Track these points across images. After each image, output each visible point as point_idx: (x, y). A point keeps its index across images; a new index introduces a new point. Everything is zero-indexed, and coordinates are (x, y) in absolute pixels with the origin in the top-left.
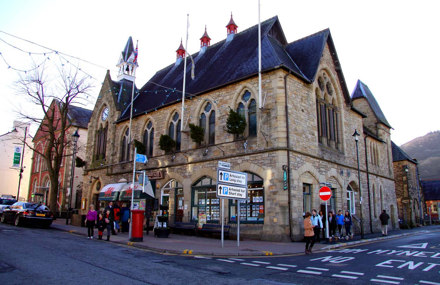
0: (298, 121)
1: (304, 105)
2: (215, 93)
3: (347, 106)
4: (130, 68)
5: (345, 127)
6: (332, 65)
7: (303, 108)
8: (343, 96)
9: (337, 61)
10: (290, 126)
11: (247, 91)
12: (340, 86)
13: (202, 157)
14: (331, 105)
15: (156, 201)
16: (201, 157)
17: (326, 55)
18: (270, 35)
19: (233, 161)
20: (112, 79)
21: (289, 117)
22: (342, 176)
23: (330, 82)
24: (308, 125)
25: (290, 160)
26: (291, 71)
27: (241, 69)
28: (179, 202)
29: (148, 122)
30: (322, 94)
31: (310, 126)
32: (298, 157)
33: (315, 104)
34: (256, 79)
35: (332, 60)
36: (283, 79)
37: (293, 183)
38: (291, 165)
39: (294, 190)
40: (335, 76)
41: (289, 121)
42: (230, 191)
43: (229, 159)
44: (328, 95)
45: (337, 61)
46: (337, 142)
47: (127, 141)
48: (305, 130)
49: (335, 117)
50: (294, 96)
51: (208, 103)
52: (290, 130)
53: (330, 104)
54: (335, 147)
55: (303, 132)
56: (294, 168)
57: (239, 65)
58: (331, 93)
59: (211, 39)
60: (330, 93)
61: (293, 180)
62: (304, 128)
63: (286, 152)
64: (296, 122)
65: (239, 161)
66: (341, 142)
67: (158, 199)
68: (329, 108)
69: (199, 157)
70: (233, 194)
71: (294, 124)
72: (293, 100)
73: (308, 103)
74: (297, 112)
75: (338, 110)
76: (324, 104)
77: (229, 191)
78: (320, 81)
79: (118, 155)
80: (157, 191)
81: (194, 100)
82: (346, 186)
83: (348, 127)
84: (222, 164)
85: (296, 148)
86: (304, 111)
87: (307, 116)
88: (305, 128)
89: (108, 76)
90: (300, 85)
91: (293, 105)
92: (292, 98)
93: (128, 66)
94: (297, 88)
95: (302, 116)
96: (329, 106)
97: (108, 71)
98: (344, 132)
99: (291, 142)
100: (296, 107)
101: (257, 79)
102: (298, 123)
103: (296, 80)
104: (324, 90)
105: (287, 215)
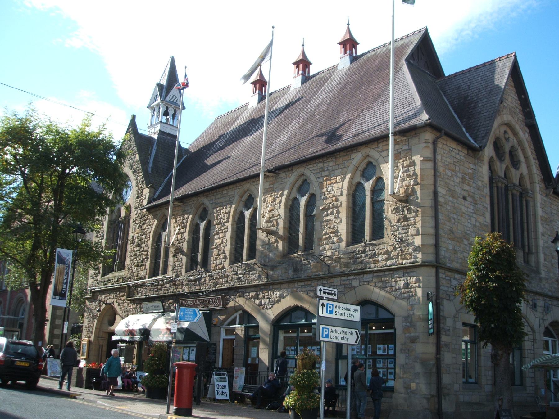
0: (455, 217)
1: (466, 187)
2: (315, 165)
3: (547, 188)
4: (171, 112)
5: (542, 224)
6: (521, 116)
7: (466, 194)
8: (540, 170)
9: (528, 110)
10: (441, 226)
11: (370, 163)
12: (534, 152)
13: (292, 273)
14: (516, 187)
15: (212, 347)
16: (291, 273)
17: (510, 99)
18: (414, 60)
19: (344, 283)
20: (140, 131)
21: (439, 211)
22: (535, 312)
23: (517, 146)
24: (474, 223)
25: (441, 284)
26: (445, 131)
27: (361, 124)
28: (252, 351)
29: (201, 210)
30: (500, 168)
31: (478, 224)
32: (454, 279)
33: (488, 186)
34: (385, 143)
35: (520, 107)
36: (430, 145)
37: (445, 323)
38: (441, 292)
39: (446, 335)
40: (524, 136)
41: (440, 216)
42: (336, 310)
43: (337, 281)
44: (513, 170)
45: (528, 110)
46: (527, 250)
47: (163, 241)
48: (468, 232)
49: (525, 208)
50: (449, 173)
51: (305, 181)
52: (441, 232)
53: (514, 185)
54: (522, 259)
55: (466, 236)
56: (448, 298)
57: (358, 116)
58: (517, 164)
59: (311, 64)
60: (515, 164)
61: (445, 318)
62: (465, 227)
63: (433, 270)
64: (452, 219)
65: (355, 283)
66: (534, 251)
67: (215, 345)
68: (514, 192)
69: (287, 274)
70: (341, 314)
71: (449, 221)
72: (448, 181)
73: (474, 185)
74: (455, 201)
75: (529, 195)
76: (503, 186)
77: (334, 310)
78: (498, 145)
79: (148, 264)
80: (214, 330)
81: (281, 176)
82: (543, 329)
83: (548, 225)
84: (325, 291)
85: (451, 264)
86: (468, 199)
87: (472, 207)
88: (468, 229)
89: (133, 124)
90: (460, 153)
91: (447, 189)
92: (446, 177)
93: (167, 108)
94: (455, 160)
95: (463, 208)
96: (514, 189)
97: (134, 117)
98: (540, 234)
99: (442, 253)
100: (452, 193)
101: (387, 143)
102: (456, 220)
103: (453, 145)
104: (504, 160)
105: (434, 378)
